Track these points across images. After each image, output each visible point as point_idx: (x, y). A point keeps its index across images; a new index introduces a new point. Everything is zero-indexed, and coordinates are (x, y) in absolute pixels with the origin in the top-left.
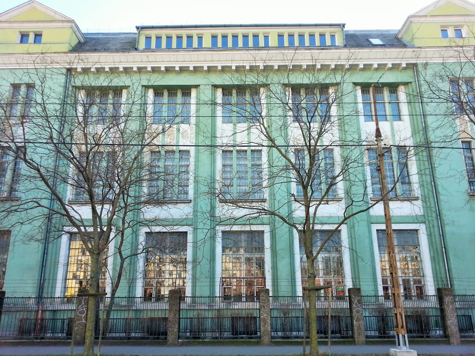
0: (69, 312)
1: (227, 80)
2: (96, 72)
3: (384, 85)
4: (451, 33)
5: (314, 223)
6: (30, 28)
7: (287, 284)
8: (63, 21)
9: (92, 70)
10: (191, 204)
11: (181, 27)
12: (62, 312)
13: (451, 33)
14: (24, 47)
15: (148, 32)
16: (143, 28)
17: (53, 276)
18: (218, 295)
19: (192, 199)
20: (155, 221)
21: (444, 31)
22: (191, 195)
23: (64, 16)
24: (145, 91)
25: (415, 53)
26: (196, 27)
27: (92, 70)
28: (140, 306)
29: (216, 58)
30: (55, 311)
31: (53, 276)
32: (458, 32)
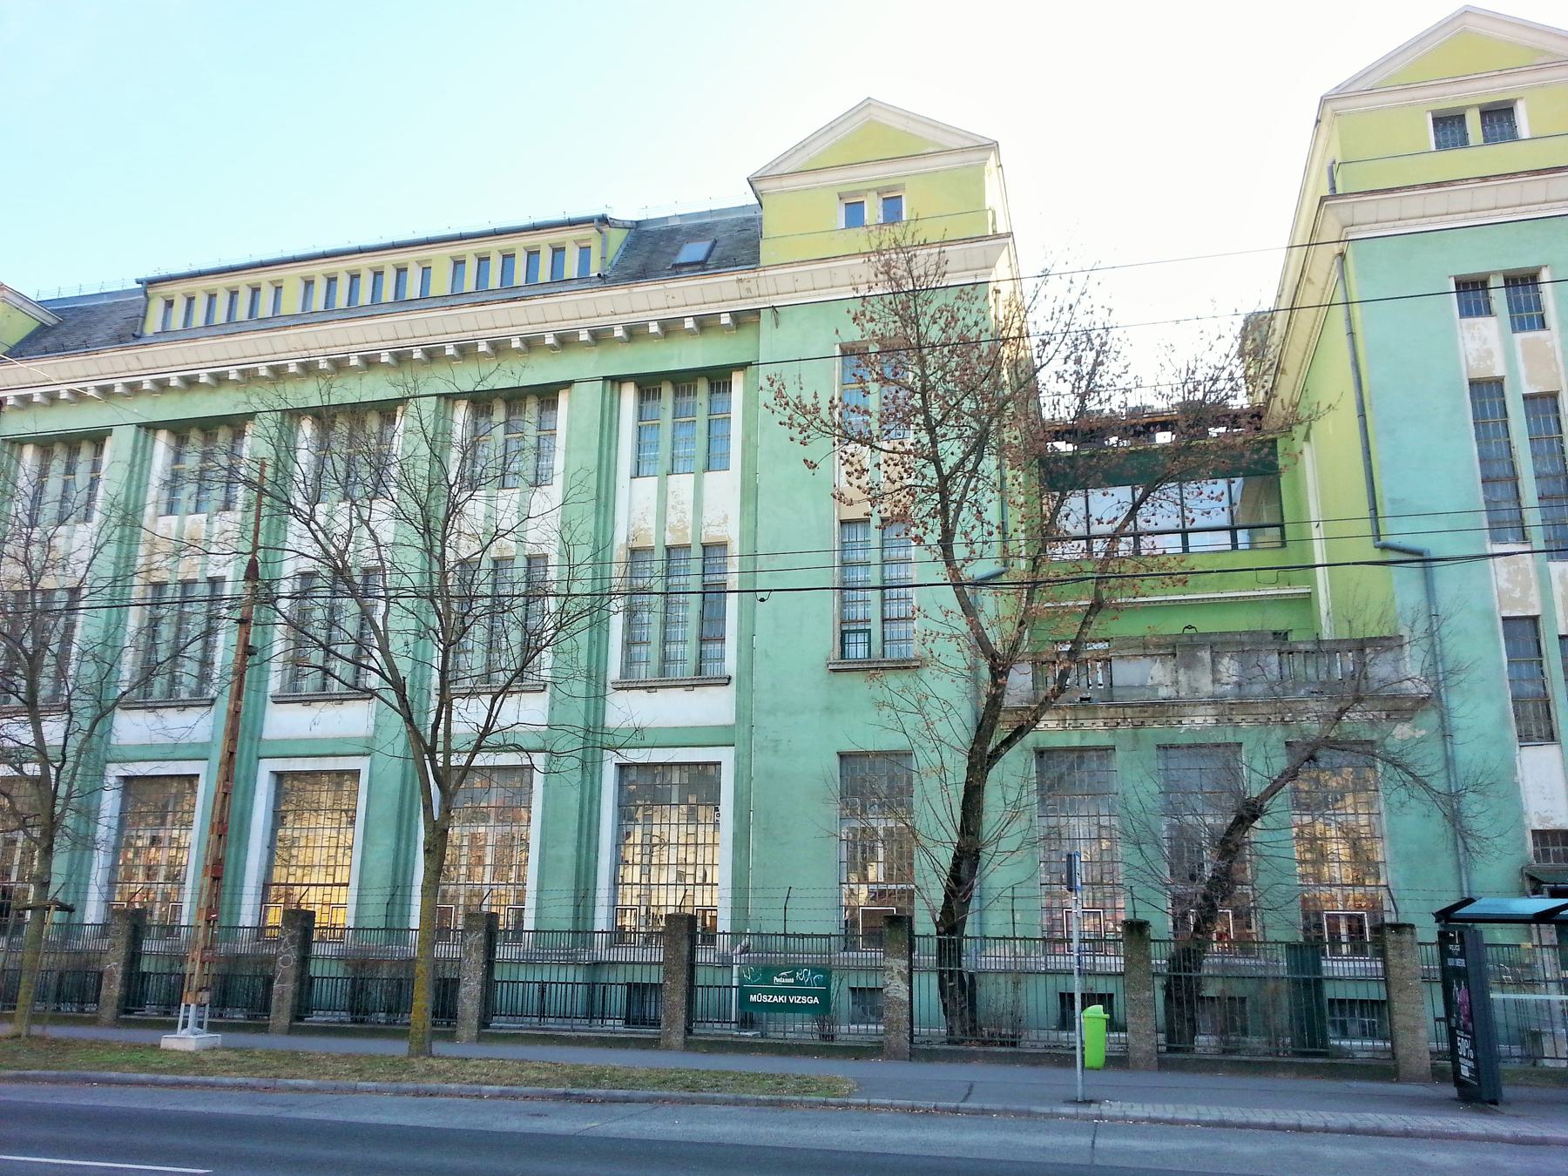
0: (629, 968)
1: (467, 378)
2: (392, 362)
3: (494, 394)
4: (873, 211)
5: (448, 753)
6: (1472, 95)
7: (379, 899)
8: (963, 150)
9: (481, 349)
10: (546, 695)
11: (461, 238)
12: (621, 967)
13: (873, 211)
14: (1456, 162)
15: (167, 289)
16: (152, 282)
17: (404, 879)
18: (184, 922)
19: (734, 676)
20: (638, 737)
21: (854, 213)
22: (731, 666)
23: (967, 135)
24: (146, 437)
25: (745, 285)
26: (263, 265)
27: (481, 349)
28: (604, 955)
29: (640, 303)
30: (597, 964)
31: (404, 879)
32: (892, 207)
